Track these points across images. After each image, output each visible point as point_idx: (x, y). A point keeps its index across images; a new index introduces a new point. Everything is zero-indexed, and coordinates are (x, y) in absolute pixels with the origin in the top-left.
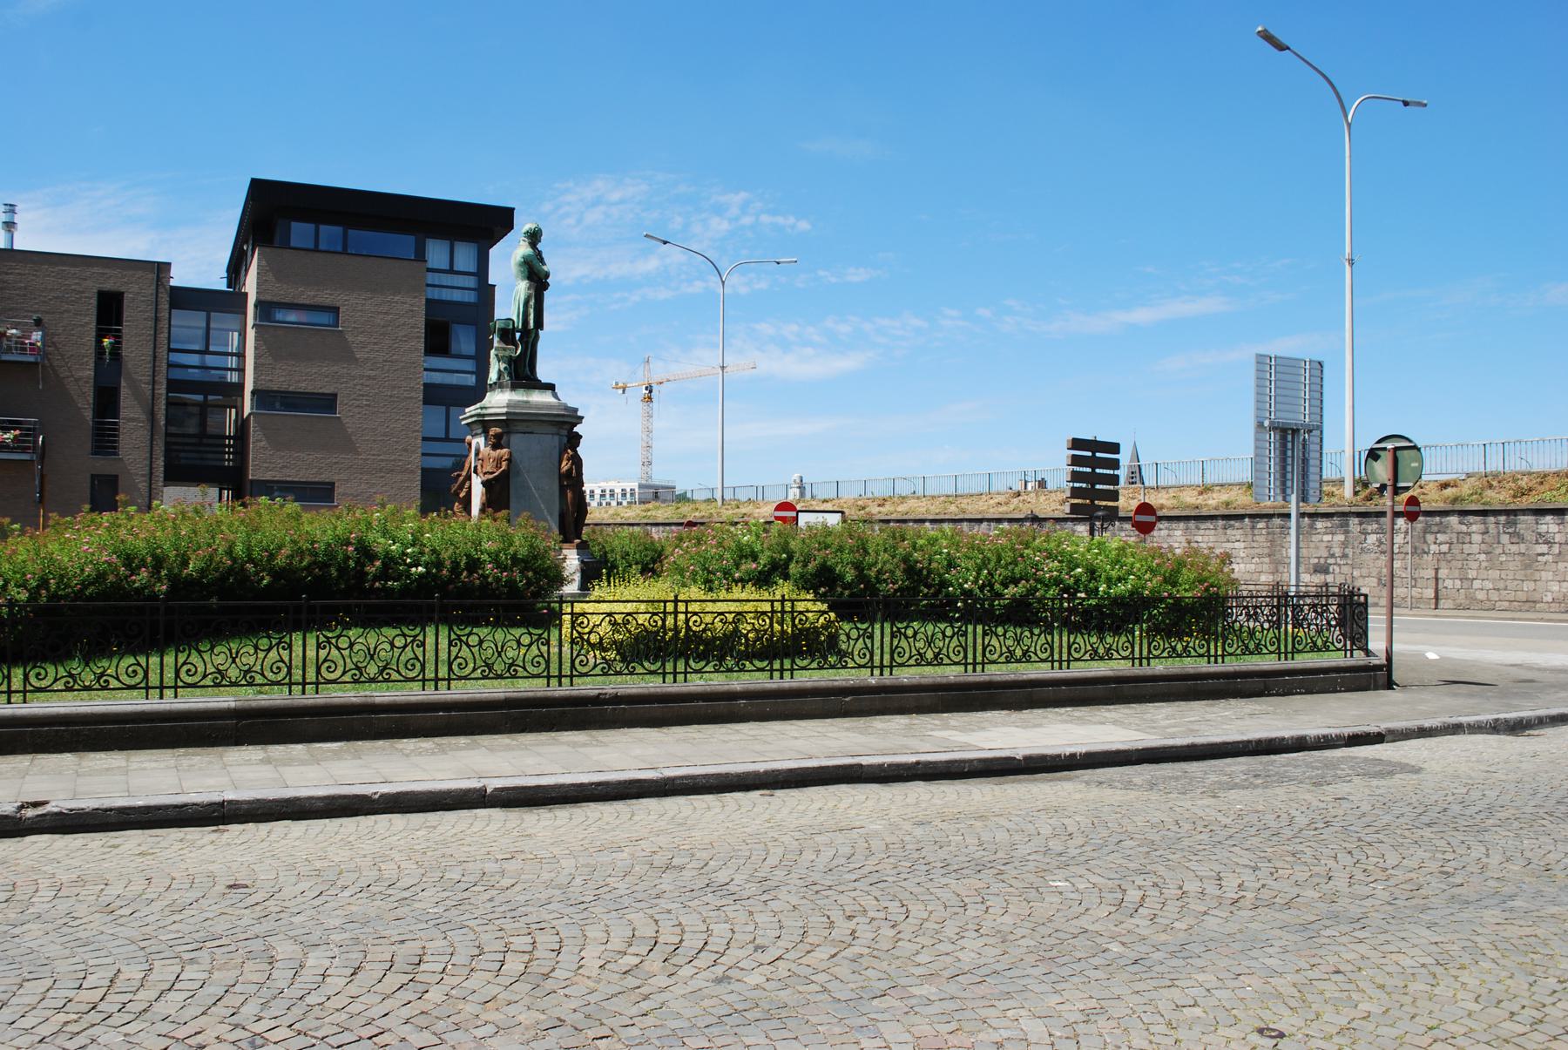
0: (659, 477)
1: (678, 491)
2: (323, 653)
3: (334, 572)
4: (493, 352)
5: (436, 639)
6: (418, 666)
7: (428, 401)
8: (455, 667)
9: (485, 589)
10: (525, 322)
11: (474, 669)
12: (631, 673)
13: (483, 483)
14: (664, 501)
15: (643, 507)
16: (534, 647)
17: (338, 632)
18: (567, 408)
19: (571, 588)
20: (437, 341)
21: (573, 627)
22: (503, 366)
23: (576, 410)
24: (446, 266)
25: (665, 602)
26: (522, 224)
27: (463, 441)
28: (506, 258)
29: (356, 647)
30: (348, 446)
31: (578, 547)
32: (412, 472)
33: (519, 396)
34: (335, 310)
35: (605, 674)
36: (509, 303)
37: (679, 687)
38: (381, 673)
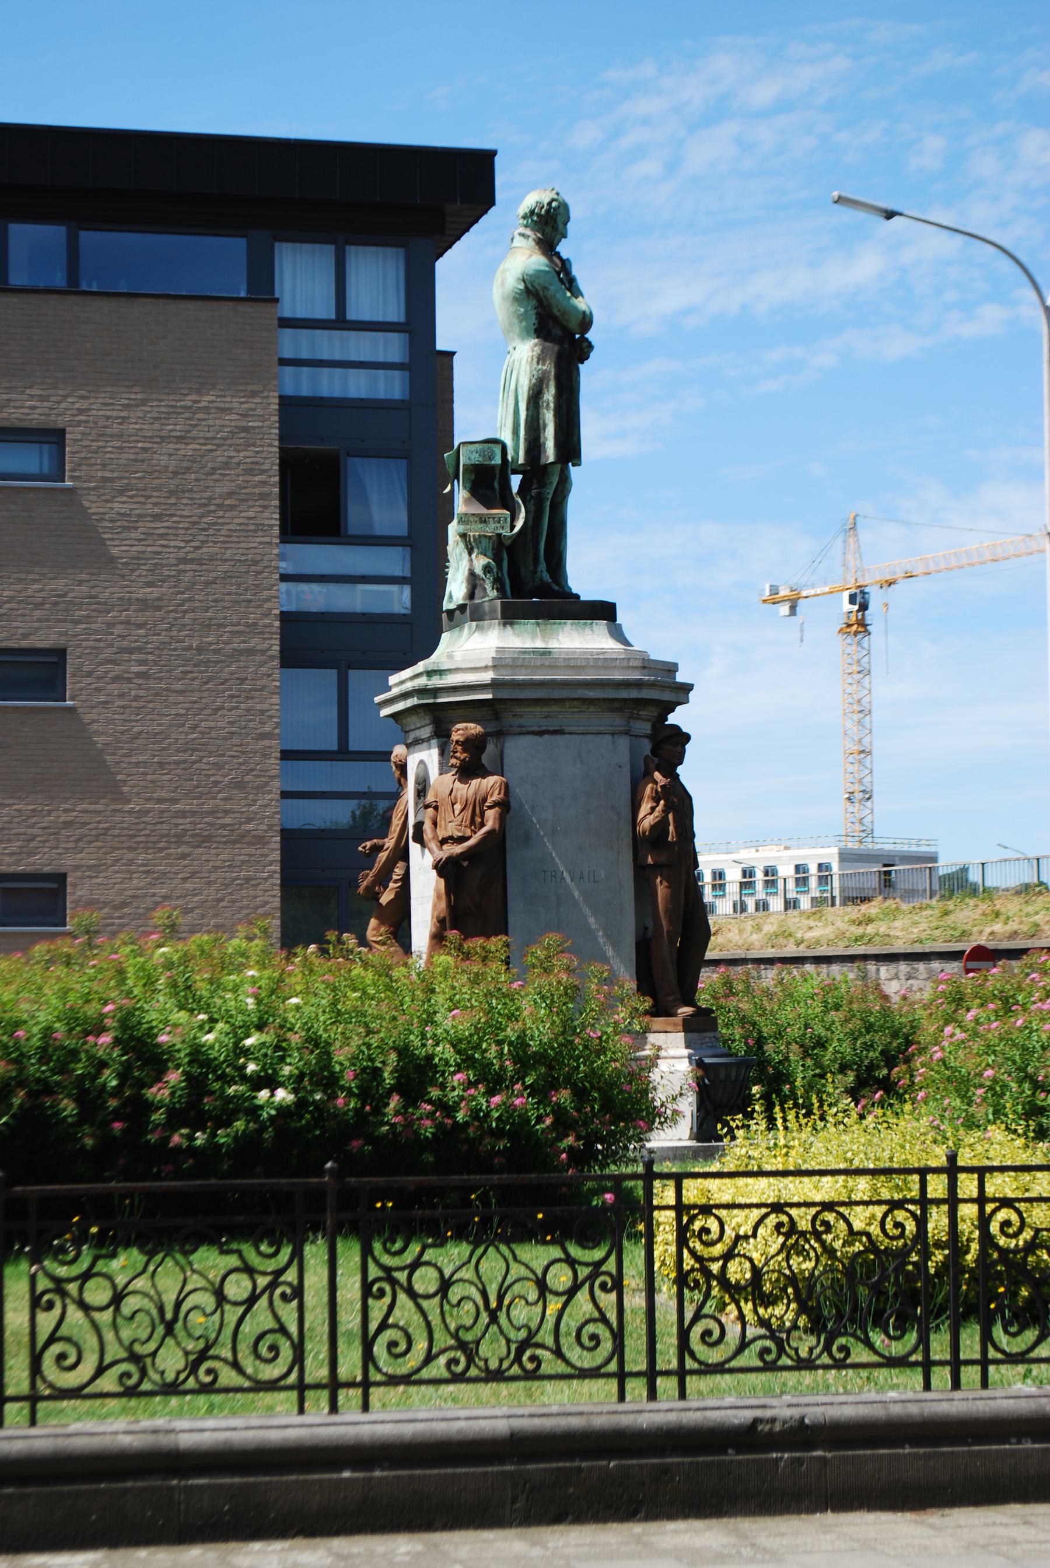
0: (894, 830)
1: (946, 865)
2: (46, 1321)
3: (68, 1107)
4: (453, 529)
5: (331, 1274)
6: (286, 1352)
7: (290, 659)
8: (379, 1349)
9: (456, 1146)
10: (534, 446)
11: (429, 1358)
12: (839, 1365)
13: (442, 868)
14: (910, 894)
15: (854, 912)
16: (582, 1296)
17: (84, 1264)
18: (647, 664)
19: (674, 1135)
20: (312, 504)
21: (682, 1241)
22: (480, 562)
23: (672, 668)
24: (326, 310)
25: (923, 1172)
26: (518, 193)
27: (385, 756)
28: (480, 282)
29: (130, 1304)
30: (97, 779)
31: (689, 1027)
32: (260, 841)
33: (523, 638)
34: (54, 438)
35: (770, 1367)
36: (491, 399)
37: (969, 1401)
38: (193, 1368)
